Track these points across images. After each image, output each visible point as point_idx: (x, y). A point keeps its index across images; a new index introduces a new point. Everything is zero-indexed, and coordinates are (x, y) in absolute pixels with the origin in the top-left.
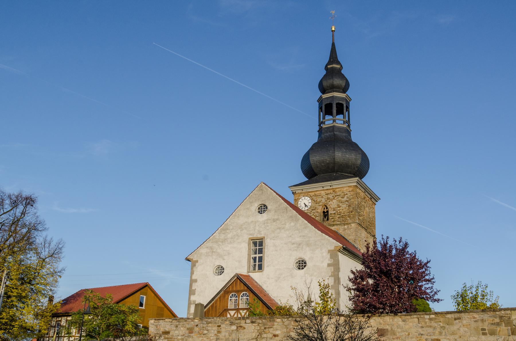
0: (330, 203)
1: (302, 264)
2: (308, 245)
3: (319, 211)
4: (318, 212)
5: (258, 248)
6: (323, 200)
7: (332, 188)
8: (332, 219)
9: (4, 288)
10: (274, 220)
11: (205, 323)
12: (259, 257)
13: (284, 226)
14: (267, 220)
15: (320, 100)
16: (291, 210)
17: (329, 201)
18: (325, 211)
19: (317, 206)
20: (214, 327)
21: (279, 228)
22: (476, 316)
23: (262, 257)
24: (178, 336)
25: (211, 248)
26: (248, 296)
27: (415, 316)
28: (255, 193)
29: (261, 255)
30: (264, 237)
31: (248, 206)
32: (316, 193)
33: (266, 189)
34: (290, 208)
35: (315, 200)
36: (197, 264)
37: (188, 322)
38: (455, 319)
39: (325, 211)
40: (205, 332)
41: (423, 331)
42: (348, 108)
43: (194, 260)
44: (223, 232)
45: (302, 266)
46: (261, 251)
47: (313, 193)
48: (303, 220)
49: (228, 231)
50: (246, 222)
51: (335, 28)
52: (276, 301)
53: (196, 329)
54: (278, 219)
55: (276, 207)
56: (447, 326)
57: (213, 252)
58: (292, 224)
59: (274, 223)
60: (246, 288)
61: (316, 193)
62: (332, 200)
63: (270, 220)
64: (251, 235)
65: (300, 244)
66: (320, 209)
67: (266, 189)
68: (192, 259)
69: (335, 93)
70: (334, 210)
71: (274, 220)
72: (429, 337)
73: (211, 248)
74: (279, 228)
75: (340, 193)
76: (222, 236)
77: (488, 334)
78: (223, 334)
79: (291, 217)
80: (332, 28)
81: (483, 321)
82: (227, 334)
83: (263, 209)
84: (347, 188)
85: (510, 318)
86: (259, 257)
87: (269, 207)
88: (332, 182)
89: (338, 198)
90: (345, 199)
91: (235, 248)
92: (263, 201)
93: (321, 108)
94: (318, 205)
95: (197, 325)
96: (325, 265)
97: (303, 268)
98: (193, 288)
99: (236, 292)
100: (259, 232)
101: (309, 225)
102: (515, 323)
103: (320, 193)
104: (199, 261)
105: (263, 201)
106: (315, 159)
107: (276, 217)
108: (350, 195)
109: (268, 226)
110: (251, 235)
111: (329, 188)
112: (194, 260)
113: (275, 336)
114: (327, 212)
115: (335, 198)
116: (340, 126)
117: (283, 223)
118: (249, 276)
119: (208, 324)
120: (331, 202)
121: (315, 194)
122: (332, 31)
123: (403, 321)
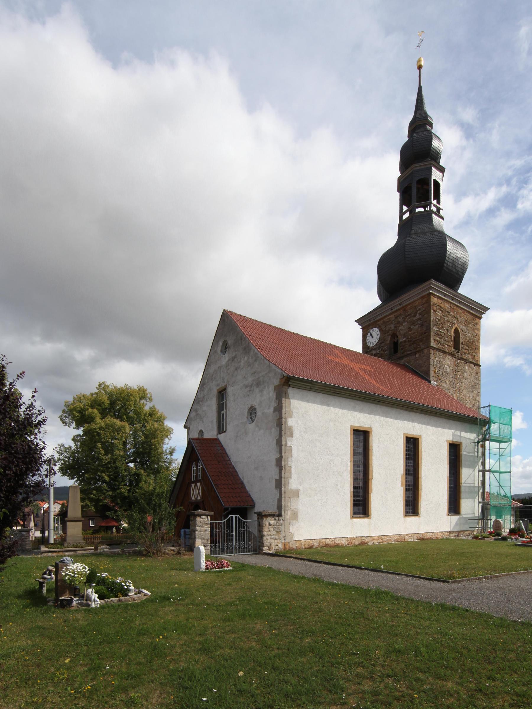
0: (400, 328)
3: (388, 342)
6: (392, 326)
7: (401, 306)
9: (96, 549)
17: (399, 326)
32: (384, 320)
61: (385, 320)
69: (414, 165)
84: (420, 301)
88: (401, 298)
89: (410, 318)
90: (418, 316)
91: (397, 599)
94: (386, 335)
96: (272, 410)
102: (526, 476)
103: (389, 318)
108: (423, 309)
111: (399, 307)
115: (406, 319)
116: (431, 190)
121: (384, 322)
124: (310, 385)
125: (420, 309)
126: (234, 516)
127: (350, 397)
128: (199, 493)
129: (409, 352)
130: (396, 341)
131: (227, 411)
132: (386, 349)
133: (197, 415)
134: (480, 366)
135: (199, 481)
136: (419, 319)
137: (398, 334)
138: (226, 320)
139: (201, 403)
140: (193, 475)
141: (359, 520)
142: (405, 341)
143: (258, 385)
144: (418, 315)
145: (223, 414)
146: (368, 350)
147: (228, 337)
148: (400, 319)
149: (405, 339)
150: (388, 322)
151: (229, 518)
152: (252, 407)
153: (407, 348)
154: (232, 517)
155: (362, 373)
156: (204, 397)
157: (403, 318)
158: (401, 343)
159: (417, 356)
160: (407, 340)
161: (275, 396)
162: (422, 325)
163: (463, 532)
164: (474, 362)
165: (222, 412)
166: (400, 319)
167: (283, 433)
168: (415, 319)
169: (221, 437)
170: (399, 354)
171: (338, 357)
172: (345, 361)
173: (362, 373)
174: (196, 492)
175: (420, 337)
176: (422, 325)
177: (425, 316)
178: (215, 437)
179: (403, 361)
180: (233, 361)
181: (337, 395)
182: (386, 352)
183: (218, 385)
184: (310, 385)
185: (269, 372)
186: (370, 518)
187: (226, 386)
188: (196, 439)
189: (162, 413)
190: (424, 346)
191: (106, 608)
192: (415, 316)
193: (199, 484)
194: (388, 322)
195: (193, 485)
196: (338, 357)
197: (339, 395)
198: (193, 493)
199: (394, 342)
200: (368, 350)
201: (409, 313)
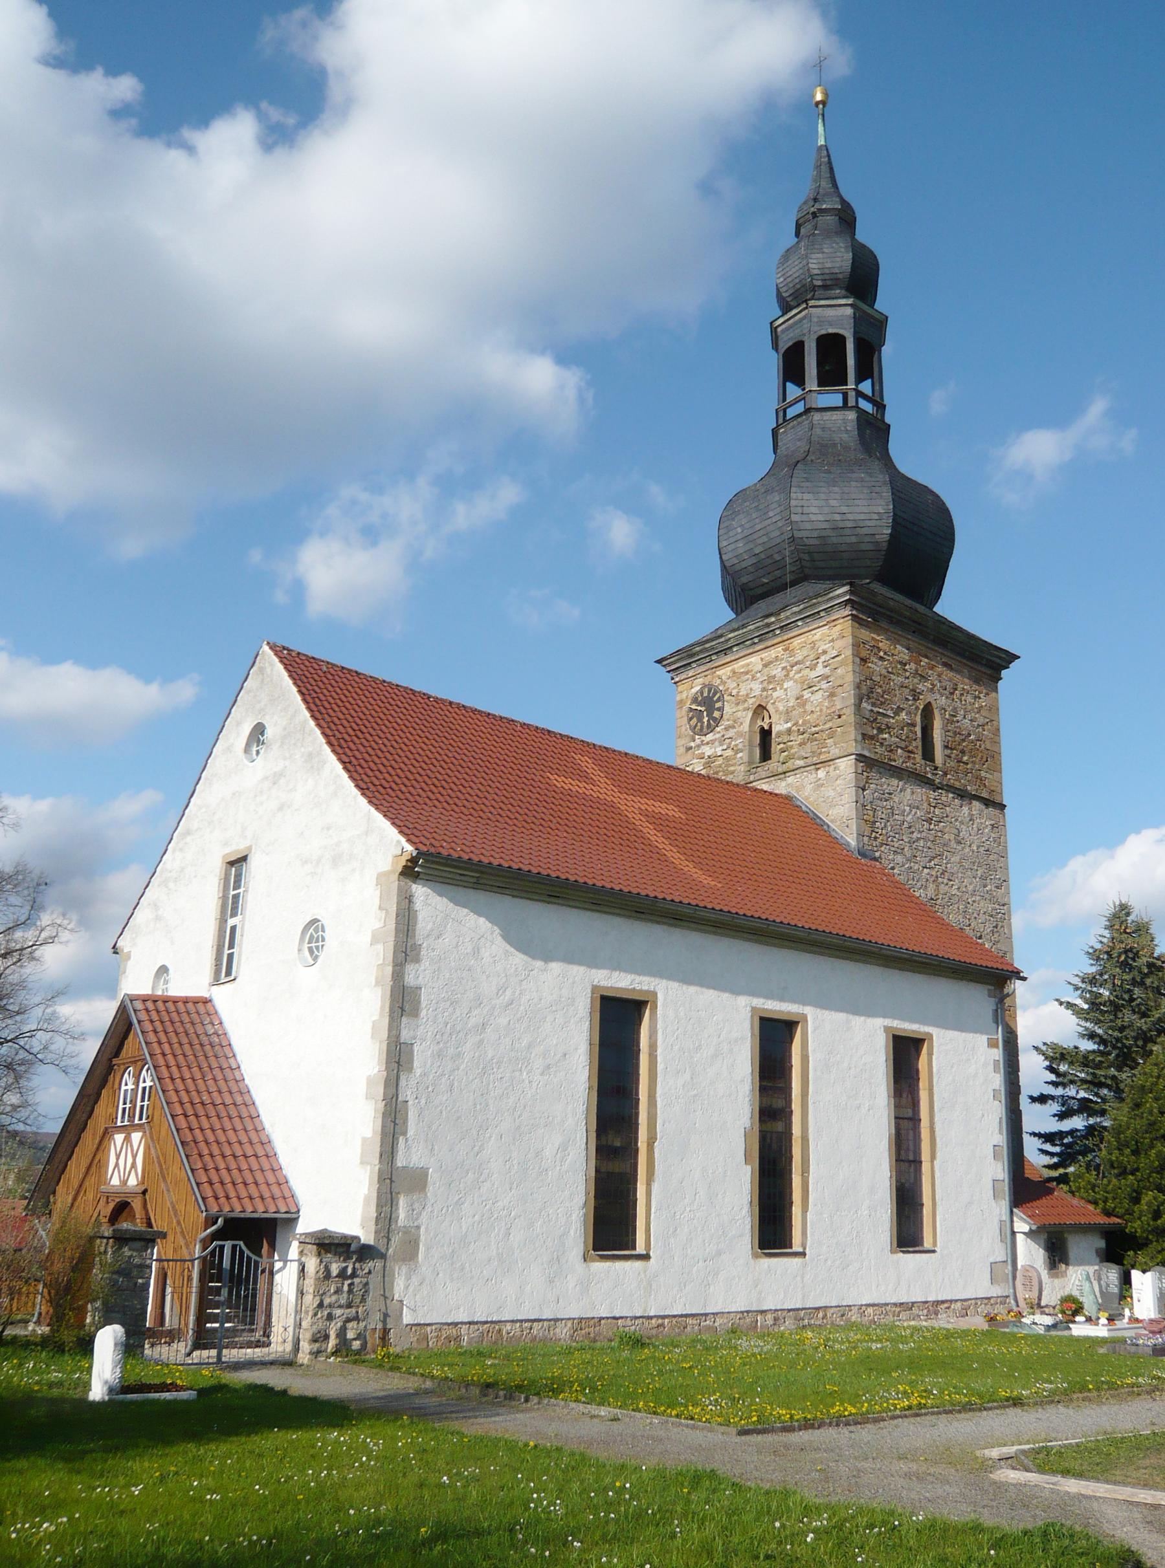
0: (775, 695)
3: (746, 727)
4: (739, 734)
6: (756, 687)
17: (774, 689)
30: (250, 848)
64: (226, 844)
67: (272, 665)
75: (805, 653)
80: (813, 96)
94: (741, 707)
108: (835, 653)
115: (792, 674)
124: (478, 875)
125: (825, 652)
126: (228, 1245)
127: (594, 907)
128: (134, 1165)
129: (801, 763)
130: (766, 728)
131: (244, 918)
132: (740, 746)
133: (158, 918)
134: (1002, 807)
135: (140, 1127)
136: (825, 677)
137: (770, 707)
138: (268, 670)
139: (171, 885)
140: (121, 1106)
142: (789, 731)
143: (336, 861)
144: (820, 666)
145: (233, 929)
146: (693, 744)
147: (267, 717)
148: (777, 671)
149: (789, 725)
150: (747, 673)
151: (214, 1250)
152: (315, 921)
153: (793, 751)
154: (222, 1248)
155: (649, 831)
156: (183, 869)
157: (783, 668)
158: (779, 735)
159: (821, 774)
160: (794, 728)
161: (377, 902)
162: (832, 695)
163: (946, 1305)
164: (985, 795)
165: (231, 922)
166: (777, 671)
168: (813, 674)
169: (224, 999)
170: (773, 765)
171: (584, 777)
172: (604, 789)
173: (649, 831)
174: (125, 1161)
175: (827, 726)
176: (832, 695)
177: (839, 671)
178: (205, 994)
179: (783, 784)
180: (275, 783)
181: (552, 899)
182: (740, 755)
183: (226, 844)
184: (478, 875)
185: (367, 834)
186: (755, 1256)
187: (250, 848)
188: (145, 999)
189: (42, 873)
190: (837, 751)
192: (812, 668)
193: (136, 1137)
194: (747, 673)
195: (119, 1138)
196: (584, 777)
197: (560, 901)
198: (117, 1165)
199: (762, 729)
200: (693, 744)
201: (799, 657)
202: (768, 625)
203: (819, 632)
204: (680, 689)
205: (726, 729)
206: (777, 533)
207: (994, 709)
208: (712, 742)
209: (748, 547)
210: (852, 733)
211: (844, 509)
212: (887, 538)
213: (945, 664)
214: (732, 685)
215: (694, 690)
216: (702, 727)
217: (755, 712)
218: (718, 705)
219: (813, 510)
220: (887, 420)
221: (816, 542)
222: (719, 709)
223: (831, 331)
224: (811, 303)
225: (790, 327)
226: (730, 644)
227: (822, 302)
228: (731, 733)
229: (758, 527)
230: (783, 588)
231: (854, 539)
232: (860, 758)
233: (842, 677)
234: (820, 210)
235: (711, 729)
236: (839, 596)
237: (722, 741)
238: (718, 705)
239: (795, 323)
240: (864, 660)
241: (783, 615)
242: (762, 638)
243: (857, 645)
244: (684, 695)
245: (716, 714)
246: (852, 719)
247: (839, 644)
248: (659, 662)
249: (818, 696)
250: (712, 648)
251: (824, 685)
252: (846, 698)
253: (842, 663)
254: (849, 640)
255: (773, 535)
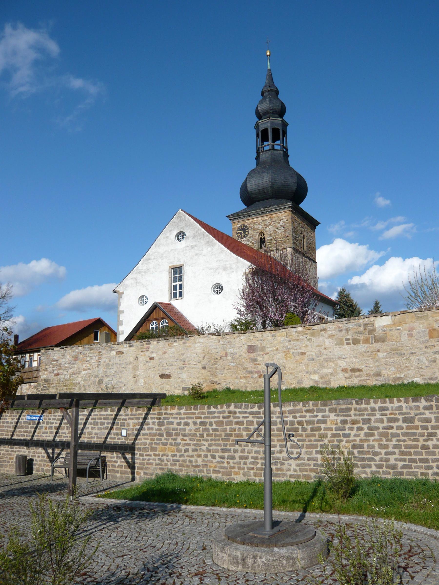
0: (266, 229)
1: (219, 288)
2: (225, 269)
3: (257, 237)
4: (255, 239)
5: (178, 275)
6: (260, 227)
8: (269, 245)
10: (192, 247)
11: (88, 350)
12: (179, 285)
13: (202, 252)
14: (186, 247)
15: (257, 127)
16: (207, 235)
17: (266, 228)
18: (263, 238)
19: (254, 234)
20: (96, 353)
21: (197, 255)
22: (340, 326)
23: (182, 284)
24: (65, 364)
25: (135, 279)
26: (167, 323)
27: (283, 330)
28: (174, 221)
29: (181, 283)
30: (183, 265)
31: (168, 235)
33: (184, 216)
34: (207, 233)
35: (252, 227)
36: (123, 296)
37: (73, 350)
38: (322, 330)
39: (263, 238)
40: (88, 359)
41: (290, 344)
42: (284, 133)
43: (120, 291)
44: (146, 262)
45: (219, 290)
46: (181, 279)
47: (250, 221)
48: (220, 244)
49: (150, 261)
50: (166, 251)
51: (270, 53)
52: (381, 343)
53: (81, 356)
54: (195, 246)
55: (194, 234)
56: (313, 338)
57: (137, 282)
58: (209, 249)
59: (192, 250)
60: (165, 316)
62: (268, 226)
63: (188, 246)
64: (171, 263)
65: (217, 269)
66: (257, 235)
67: (184, 216)
68: (119, 291)
70: (270, 235)
71: (192, 247)
72: (296, 351)
73: (135, 279)
74: (197, 255)
75: (276, 219)
76: (145, 267)
77: (351, 343)
78: (104, 359)
79: (208, 242)
80: (267, 53)
81: (347, 330)
82: (107, 360)
83: (180, 236)
85: (374, 326)
86: (179, 285)
87: (187, 234)
89: (274, 224)
90: (281, 224)
92: (181, 228)
93: (257, 136)
94: (255, 232)
95: (81, 353)
97: (220, 293)
98: (121, 319)
99: (156, 320)
100: (179, 260)
101: (225, 249)
104: (125, 293)
105: (181, 228)
106: (252, 186)
107: (194, 244)
108: (286, 220)
109: (187, 253)
110: (171, 263)
112: (120, 291)
113: (151, 359)
114: (264, 238)
115: (272, 224)
117: (200, 249)
118: (170, 304)
119: (91, 350)
120: (267, 229)
121: (252, 222)
122: (268, 56)
123: (272, 336)
125: (282, 219)
136: (283, 226)
141: (168, 289)
142: (271, 240)
144: (281, 223)
148: (267, 223)
150: (257, 222)
158: (268, 240)
162: (285, 231)
166: (267, 223)
167: (373, 382)
168: (279, 225)
176: (285, 231)
177: (287, 225)
187: (183, 265)
191: (347, 423)
192: (279, 223)
194: (257, 222)
202: (265, 210)
203: (281, 214)
204: (233, 225)
205: (250, 237)
206: (267, 185)
207: (314, 237)
208: (245, 241)
209: (256, 187)
210: (292, 242)
211: (285, 180)
212: (295, 189)
213: (307, 224)
214: (251, 225)
215: (238, 226)
216: (242, 236)
217: (260, 234)
218: (247, 231)
219: (277, 180)
220: (289, 154)
221: (277, 188)
222: (247, 232)
223: (276, 127)
224: (271, 118)
225: (263, 124)
226: (252, 214)
227: (274, 118)
228: (252, 239)
229: (260, 182)
230: (269, 199)
231: (287, 189)
232: (294, 248)
233: (288, 227)
234: (271, 90)
235: (245, 237)
236: (288, 205)
237: (248, 240)
238: (247, 231)
239: (266, 123)
240: (293, 223)
241: (270, 208)
242: (262, 213)
243: (292, 218)
244: (235, 227)
245: (247, 233)
246: (292, 238)
247: (287, 218)
248: (227, 217)
249: (281, 231)
250: (246, 214)
251: (282, 228)
252: (289, 232)
253: (288, 223)
254: (290, 217)
255: (265, 185)
